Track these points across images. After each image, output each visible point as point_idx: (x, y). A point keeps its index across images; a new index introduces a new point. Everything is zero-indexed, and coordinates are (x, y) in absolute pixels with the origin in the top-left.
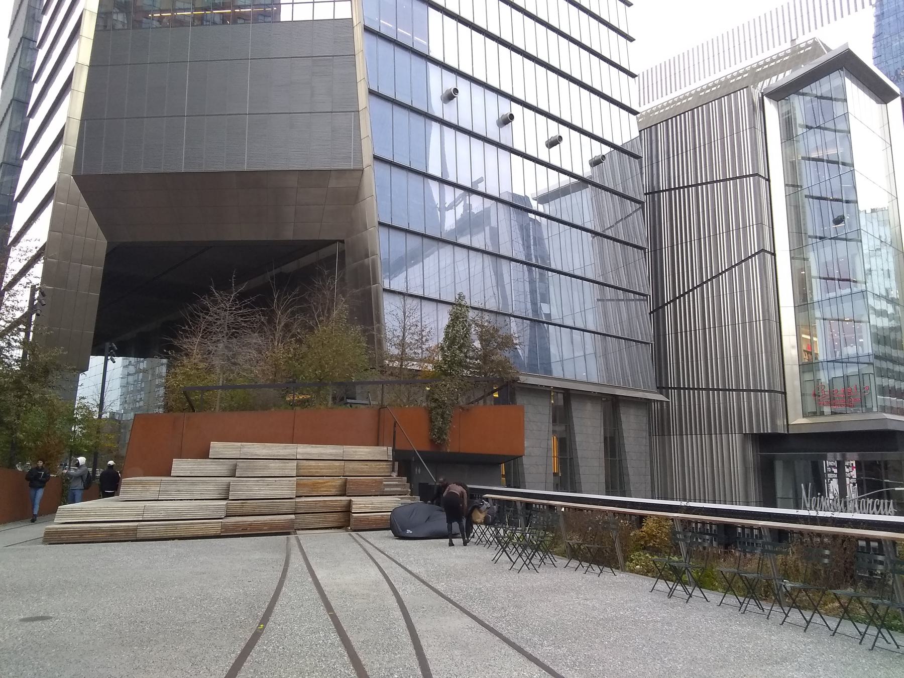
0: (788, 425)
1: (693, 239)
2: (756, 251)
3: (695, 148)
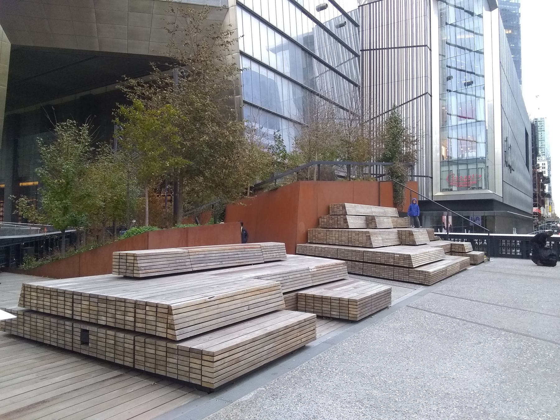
3: (388, 25)
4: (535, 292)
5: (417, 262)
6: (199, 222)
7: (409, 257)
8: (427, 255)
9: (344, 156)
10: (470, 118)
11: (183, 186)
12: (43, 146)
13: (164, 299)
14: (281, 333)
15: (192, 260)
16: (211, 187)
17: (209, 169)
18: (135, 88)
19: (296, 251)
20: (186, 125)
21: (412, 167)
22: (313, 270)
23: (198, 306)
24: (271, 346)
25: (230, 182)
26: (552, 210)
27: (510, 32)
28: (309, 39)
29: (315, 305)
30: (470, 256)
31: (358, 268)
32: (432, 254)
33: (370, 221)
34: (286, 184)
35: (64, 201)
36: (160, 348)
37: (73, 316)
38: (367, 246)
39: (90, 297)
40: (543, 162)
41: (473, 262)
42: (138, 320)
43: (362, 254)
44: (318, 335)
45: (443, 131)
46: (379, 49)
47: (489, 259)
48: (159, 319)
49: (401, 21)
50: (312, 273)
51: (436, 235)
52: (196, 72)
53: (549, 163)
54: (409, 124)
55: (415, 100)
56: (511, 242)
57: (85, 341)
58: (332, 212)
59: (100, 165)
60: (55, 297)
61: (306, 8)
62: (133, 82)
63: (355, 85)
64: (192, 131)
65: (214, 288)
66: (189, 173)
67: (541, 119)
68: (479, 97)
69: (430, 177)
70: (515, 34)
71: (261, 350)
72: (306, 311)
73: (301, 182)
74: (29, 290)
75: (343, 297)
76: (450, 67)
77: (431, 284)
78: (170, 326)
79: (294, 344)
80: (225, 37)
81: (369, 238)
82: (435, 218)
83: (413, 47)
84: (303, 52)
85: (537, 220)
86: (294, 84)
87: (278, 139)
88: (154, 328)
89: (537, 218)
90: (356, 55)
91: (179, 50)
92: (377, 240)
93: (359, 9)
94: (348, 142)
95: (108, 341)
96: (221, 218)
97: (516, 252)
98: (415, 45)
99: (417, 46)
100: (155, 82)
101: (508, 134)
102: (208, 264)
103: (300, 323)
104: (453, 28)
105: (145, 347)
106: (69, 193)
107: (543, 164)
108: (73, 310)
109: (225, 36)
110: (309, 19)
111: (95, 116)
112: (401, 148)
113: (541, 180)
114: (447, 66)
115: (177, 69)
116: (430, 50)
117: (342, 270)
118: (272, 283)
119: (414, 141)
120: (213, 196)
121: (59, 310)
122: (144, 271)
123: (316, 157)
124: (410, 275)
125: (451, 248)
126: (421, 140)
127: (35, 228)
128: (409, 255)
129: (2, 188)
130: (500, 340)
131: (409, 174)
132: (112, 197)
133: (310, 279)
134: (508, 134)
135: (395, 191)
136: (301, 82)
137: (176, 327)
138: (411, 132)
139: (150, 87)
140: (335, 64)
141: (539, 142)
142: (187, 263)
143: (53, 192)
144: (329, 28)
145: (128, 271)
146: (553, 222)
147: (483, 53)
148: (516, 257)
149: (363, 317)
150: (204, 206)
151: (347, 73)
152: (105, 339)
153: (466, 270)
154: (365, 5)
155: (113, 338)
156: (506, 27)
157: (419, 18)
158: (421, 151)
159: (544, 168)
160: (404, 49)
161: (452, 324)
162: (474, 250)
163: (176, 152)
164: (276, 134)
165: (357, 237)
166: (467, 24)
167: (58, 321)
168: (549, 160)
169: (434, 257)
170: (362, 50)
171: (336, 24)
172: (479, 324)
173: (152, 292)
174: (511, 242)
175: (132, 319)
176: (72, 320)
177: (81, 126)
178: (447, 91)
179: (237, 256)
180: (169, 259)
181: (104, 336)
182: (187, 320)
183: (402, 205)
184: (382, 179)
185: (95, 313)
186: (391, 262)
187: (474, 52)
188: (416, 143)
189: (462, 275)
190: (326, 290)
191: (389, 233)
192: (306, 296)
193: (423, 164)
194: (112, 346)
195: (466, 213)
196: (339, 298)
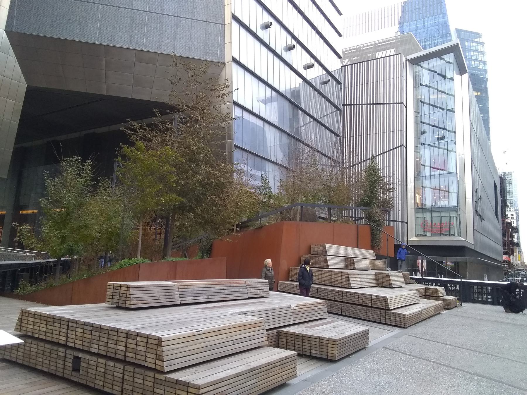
0: (408, 240)
1: (363, 134)
2: (382, 153)
3: (367, 83)
4: (506, 339)
5: (393, 304)
6: (187, 256)
7: (385, 299)
8: (403, 298)
9: (325, 199)
10: (443, 170)
11: (174, 220)
12: (48, 179)
13: (154, 331)
14: (264, 369)
15: (180, 293)
16: (200, 223)
17: (200, 206)
18: (138, 130)
19: (277, 289)
20: (182, 165)
21: (388, 212)
22: (294, 308)
23: (186, 339)
24: (254, 381)
25: (218, 219)
26: (521, 259)
27: (479, 94)
28: (296, 93)
29: (296, 342)
30: (443, 300)
31: (337, 308)
32: (407, 297)
33: (349, 262)
34: (270, 223)
35: (63, 231)
36: (148, 379)
37: (66, 343)
38: (346, 287)
39: (84, 325)
40: (512, 213)
41: (446, 307)
42: (128, 350)
43: (341, 294)
44: (298, 373)
45: (417, 180)
46: (359, 104)
47: (462, 304)
48: (149, 350)
49: (379, 81)
50: (293, 311)
51: (411, 278)
52: (194, 119)
53: (517, 214)
54: (385, 173)
55: (392, 151)
56: (482, 289)
57: (76, 368)
58: (313, 252)
59: (98, 198)
60: (52, 324)
61: (295, 66)
62: (136, 125)
63: (337, 135)
64: (187, 172)
65: (201, 322)
66: (181, 209)
67: (509, 173)
68: (450, 151)
69: (405, 223)
70: (484, 95)
71: (244, 385)
72: (286, 349)
73: (285, 222)
74: (27, 315)
75: (323, 336)
76: (424, 123)
77: (406, 327)
78: (159, 357)
79: (276, 380)
80: (221, 89)
81: (348, 278)
82: (410, 261)
83: (390, 104)
84: (290, 104)
85: (506, 267)
86: (280, 132)
87: (264, 180)
88: (143, 358)
89: (507, 266)
90: (338, 109)
91: (180, 100)
92: (355, 281)
93: (342, 68)
94: (330, 187)
95: (98, 368)
96: (207, 252)
97: (487, 298)
98: (392, 102)
99: (393, 103)
100: (156, 126)
101: (478, 186)
102: (196, 298)
103: (281, 360)
104: (426, 89)
105: (133, 377)
106: (68, 223)
107: (511, 214)
108: (67, 337)
109: (222, 88)
110: (297, 76)
111: (98, 153)
112: (378, 195)
113: (510, 230)
114: (421, 122)
115: (177, 116)
116: (406, 107)
117: (322, 309)
118: (256, 319)
119: (391, 189)
120: (200, 231)
121: (54, 336)
122: (136, 302)
123: (300, 199)
124: (386, 317)
125: (426, 292)
126: (397, 188)
127: (30, 254)
128: (386, 298)
129: (3, 215)
130: (472, 384)
131: (386, 219)
132: (107, 228)
133: (292, 317)
134: (478, 186)
135: (373, 234)
136: (288, 130)
137: (165, 359)
138: (388, 180)
139: (152, 130)
140: (318, 115)
141: (508, 194)
142: (176, 296)
143: (54, 222)
144: (314, 84)
145: (121, 302)
146: (523, 270)
147: (454, 112)
148: (487, 303)
149: (342, 356)
150: (192, 241)
151: (330, 125)
152: (95, 367)
153: (439, 313)
154: (347, 65)
155: (104, 366)
156: (475, 90)
157: (395, 79)
158: (397, 198)
159: (512, 218)
160: (382, 105)
161: (427, 367)
162: (447, 294)
163: (171, 190)
164: (263, 176)
165: (336, 277)
166: (440, 85)
167: (52, 347)
168: (518, 212)
169: (409, 300)
170: (344, 105)
171: (321, 81)
172: (452, 368)
173: (143, 323)
174: (482, 289)
175: (123, 348)
176: (65, 346)
177: (86, 162)
178: (421, 144)
179: (223, 291)
180: (160, 291)
181: (95, 364)
182: (175, 352)
183: (379, 247)
184: (361, 222)
185: (88, 340)
186: (369, 303)
187: (446, 110)
188: (392, 190)
189: (436, 318)
190: (307, 329)
191: (367, 275)
192: (287, 333)
193: (399, 211)
194: (102, 374)
195: (439, 258)
196: (319, 337)
